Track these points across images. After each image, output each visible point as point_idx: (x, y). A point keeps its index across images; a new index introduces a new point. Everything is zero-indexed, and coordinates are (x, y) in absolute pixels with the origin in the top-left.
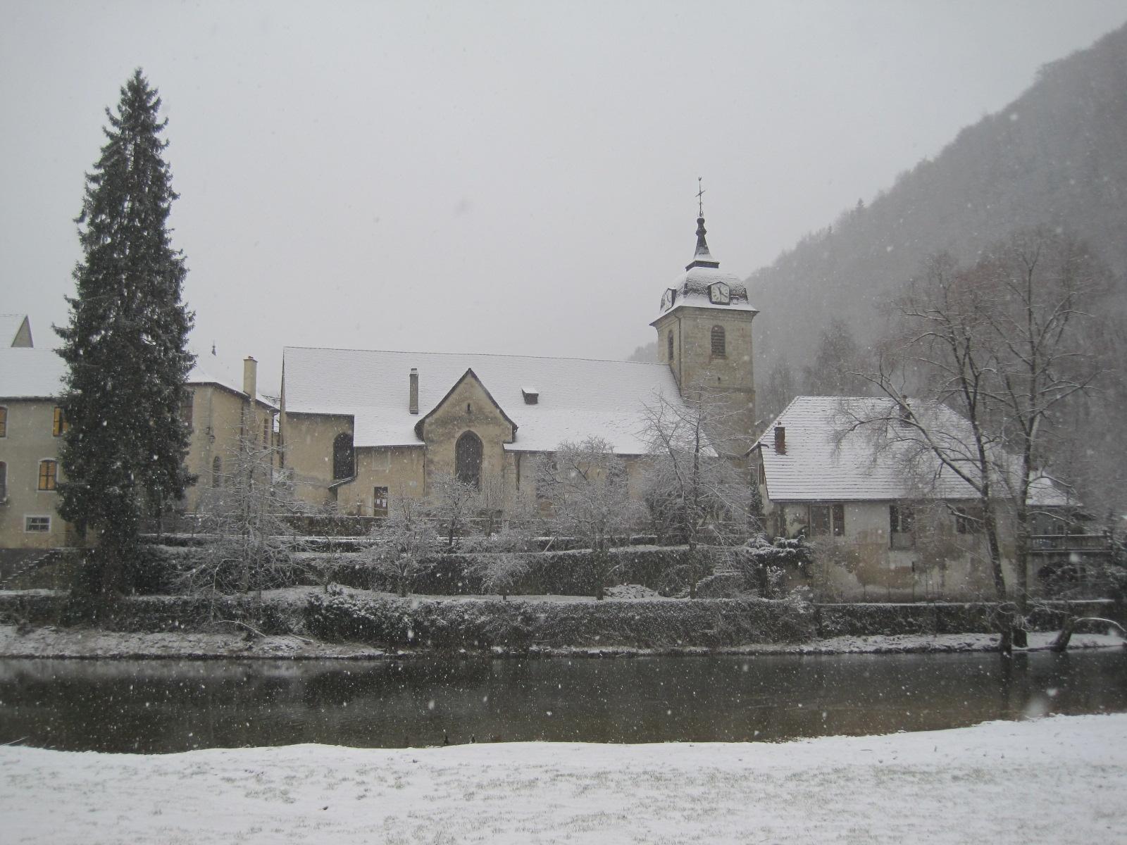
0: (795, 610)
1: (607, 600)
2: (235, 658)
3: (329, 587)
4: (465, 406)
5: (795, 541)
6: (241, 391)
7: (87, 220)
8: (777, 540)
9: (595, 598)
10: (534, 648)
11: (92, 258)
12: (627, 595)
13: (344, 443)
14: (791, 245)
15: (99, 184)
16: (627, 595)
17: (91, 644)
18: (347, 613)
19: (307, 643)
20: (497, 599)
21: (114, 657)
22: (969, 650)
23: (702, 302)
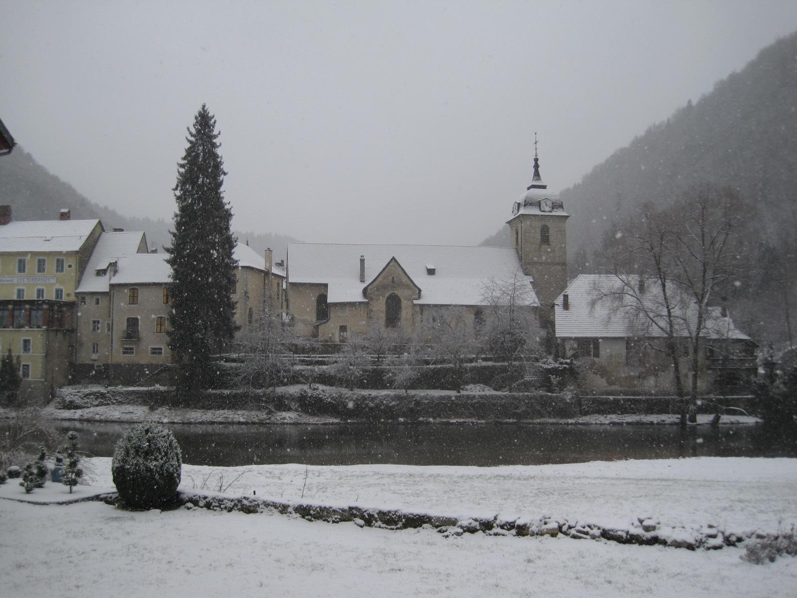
0: (565, 400)
1: (463, 393)
2: (261, 423)
3: (312, 385)
4: (391, 278)
5: (568, 361)
6: (263, 268)
7: (179, 188)
8: (558, 360)
9: (456, 392)
10: (421, 419)
11: (183, 209)
12: (475, 391)
13: (322, 298)
14: (641, 132)
15: (185, 169)
16: (475, 391)
17: (188, 416)
18: (321, 400)
19: (300, 416)
20: (402, 392)
21: (201, 423)
22: (662, 424)
23: (534, 211)
